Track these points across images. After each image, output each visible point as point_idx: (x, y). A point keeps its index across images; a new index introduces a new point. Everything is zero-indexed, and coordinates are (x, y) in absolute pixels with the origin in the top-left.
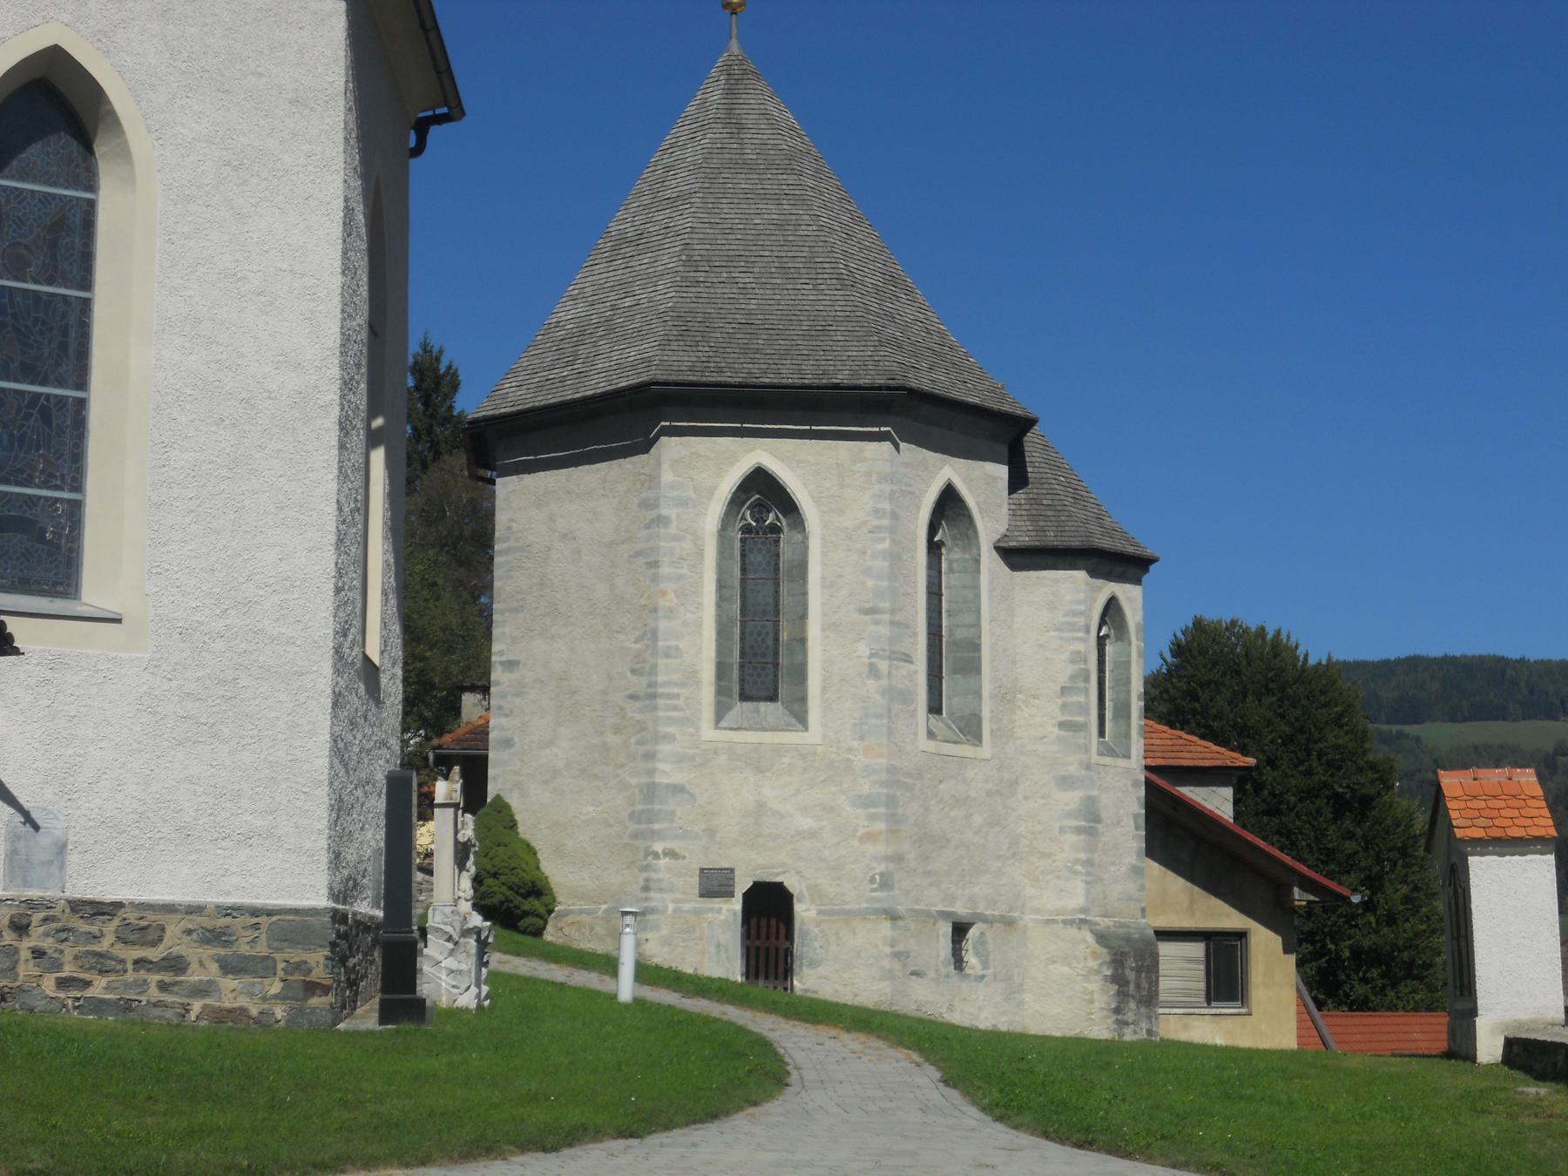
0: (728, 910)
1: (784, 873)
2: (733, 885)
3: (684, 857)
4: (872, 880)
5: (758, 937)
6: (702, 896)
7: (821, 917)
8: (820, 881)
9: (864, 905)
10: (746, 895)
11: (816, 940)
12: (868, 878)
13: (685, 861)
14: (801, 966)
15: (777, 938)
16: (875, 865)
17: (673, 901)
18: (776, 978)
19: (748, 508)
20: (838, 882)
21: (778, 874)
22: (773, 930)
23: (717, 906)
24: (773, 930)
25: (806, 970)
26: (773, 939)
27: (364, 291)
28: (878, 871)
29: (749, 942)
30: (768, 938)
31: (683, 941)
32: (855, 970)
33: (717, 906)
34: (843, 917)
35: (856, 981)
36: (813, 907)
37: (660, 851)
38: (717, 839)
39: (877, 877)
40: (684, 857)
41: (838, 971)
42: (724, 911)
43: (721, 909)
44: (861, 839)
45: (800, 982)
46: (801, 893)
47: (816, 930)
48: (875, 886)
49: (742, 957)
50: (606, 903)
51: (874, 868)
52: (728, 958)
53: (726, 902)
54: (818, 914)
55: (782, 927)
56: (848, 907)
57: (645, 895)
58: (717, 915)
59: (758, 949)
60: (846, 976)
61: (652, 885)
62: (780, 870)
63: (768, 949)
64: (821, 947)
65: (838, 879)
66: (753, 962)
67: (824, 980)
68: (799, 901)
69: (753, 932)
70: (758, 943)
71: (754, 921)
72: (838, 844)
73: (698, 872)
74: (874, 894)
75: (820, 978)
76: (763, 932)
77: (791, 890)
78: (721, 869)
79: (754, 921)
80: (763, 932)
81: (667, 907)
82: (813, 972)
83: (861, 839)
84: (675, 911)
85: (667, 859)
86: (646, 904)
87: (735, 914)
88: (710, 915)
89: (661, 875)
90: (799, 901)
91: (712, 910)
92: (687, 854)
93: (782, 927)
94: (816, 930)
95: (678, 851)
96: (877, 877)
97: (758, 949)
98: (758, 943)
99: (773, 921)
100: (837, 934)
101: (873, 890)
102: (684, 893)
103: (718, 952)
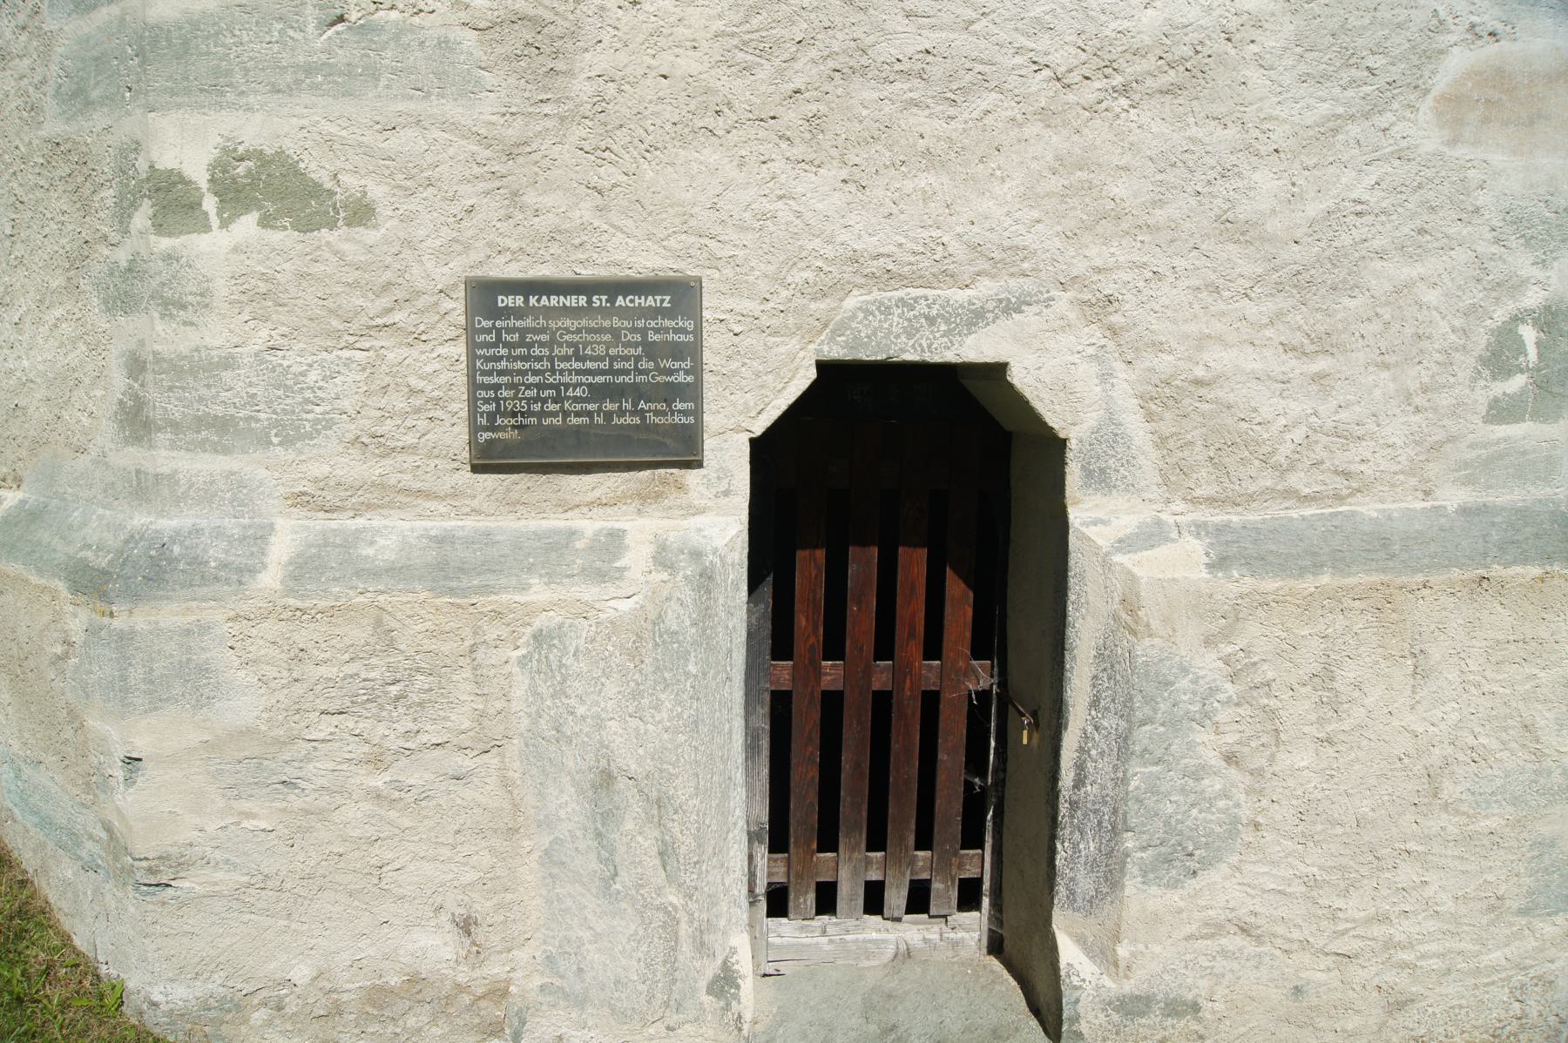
0: (663, 558)
1: (1010, 307)
2: (693, 392)
3: (361, 213)
4: (1501, 358)
5: (834, 648)
6: (487, 460)
7: (1238, 583)
8: (1219, 358)
9: (1453, 497)
10: (764, 450)
11: (1204, 717)
12: (1481, 340)
13: (370, 236)
14: (1111, 874)
15: (933, 648)
16: (1522, 263)
17: (300, 500)
18: (924, 842)
19: (590, 385)
20: (1322, 364)
21: (976, 317)
22: (911, 609)
23: (589, 525)
24: (911, 609)
25: (1139, 897)
26: (910, 645)
27: (866, 765)
28: (1533, 298)
29: (783, 671)
30: (884, 647)
31: (376, 761)
32: (1407, 873)
33: (589, 525)
34: (1360, 579)
35: (1401, 930)
36: (1178, 513)
37: (199, 174)
38: (582, 88)
39: (1528, 334)
40: (361, 213)
41: (1312, 883)
42: (637, 558)
43: (614, 541)
44: (1454, 107)
45: (1104, 955)
46: (1111, 434)
47: (1208, 665)
48: (1517, 382)
49: (751, 749)
50: (19, 482)
51: (1515, 286)
52: (665, 853)
53: (645, 498)
54: (1219, 564)
55: (957, 591)
56: (1368, 508)
57: (130, 457)
58: (589, 592)
59: (832, 703)
60: (1355, 906)
61: (164, 403)
62: (985, 289)
63: (882, 702)
64: (1230, 758)
65: (1324, 344)
66: (805, 774)
67: (1235, 942)
68: (1099, 479)
69: (808, 626)
70: (831, 673)
71: (810, 566)
72: (1331, 128)
73: (456, 307)
74: (1502, 431)
75: (1215, 929)
76: (861, 618)
77: (1053, 418)
78: (615, 288)
79: (810, 566)
80: (861, 618)
81: (260, 537)
82: (1174, 898)
83: (1454, 107)
84: (303, 569)
85: (247, 225)
86: (140, 520)
87: (706, 579)
88: (539, 592)
89: (214, 335)
90: (1099, 479)
91: (555, 548)
92: (377, 192)
93: (957, 591)
94: (1208, 665)
95: (317, 168)
96: (1528, 334)
97: (832, 703)
98: (831, 673)
99: (914, 563)
100: (1324, 676)
101: (1501, 412)
102: (372, 444)
103: (604, 819)
